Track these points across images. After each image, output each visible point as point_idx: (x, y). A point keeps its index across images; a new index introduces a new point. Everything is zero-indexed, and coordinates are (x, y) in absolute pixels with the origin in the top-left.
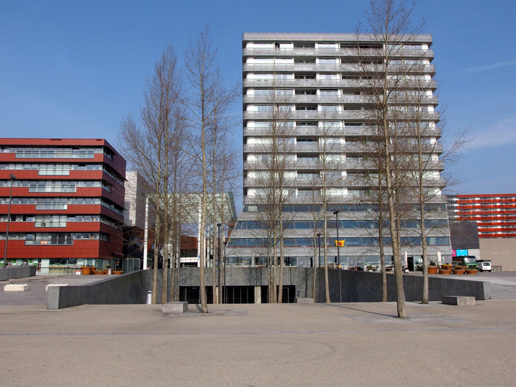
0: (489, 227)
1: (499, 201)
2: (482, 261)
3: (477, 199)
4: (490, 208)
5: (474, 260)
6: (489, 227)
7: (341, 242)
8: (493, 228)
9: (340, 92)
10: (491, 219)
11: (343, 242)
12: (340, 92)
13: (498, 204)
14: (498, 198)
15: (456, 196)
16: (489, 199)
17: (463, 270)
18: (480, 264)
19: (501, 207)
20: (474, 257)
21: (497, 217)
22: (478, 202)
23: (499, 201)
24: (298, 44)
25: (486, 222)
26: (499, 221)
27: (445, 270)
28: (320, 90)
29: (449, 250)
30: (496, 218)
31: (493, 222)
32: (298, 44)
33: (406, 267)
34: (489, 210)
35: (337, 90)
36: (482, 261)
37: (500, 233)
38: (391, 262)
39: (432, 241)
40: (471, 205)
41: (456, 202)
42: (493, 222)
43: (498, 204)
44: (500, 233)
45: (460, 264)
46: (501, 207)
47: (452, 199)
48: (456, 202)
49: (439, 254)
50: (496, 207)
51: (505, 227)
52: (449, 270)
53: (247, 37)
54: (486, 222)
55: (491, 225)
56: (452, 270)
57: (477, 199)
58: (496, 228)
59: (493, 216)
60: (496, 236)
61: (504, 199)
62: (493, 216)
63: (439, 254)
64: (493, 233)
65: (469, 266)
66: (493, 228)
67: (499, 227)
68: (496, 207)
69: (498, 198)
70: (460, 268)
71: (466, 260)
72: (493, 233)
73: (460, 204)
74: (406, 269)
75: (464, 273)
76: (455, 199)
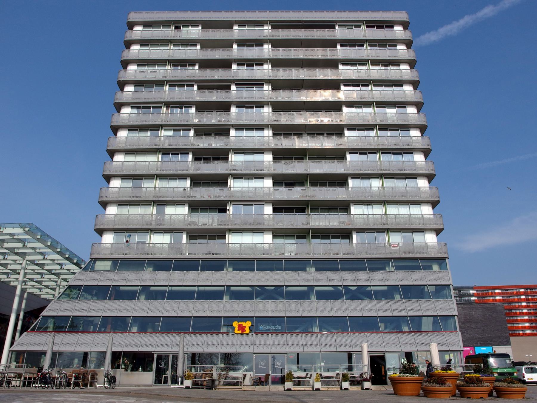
0: (515, 325)
1: (524, 294)
2: (522, 364)
3: (497, 291)
4: (514, 301)
5: (508, 361)
6: (515, 325)
7: (244, 324)
8: (520, 325)
9: (267, 88)
10: (516, 315)
11: (248, 324)
12: (267, 88)
13: (523, 297)
14: (522, 290)
15: (472, 288)
16: (511, 291)
17: (487, 386)
18: (519, 371)
19: (527, 300)
20: (506, 356)
21: (523, 313)
22: (499, 294)
23: (524, 294)
24: (207, 25)
25: (511, 318)
26: (526, 318)
27: (437, 387)
28: (236, 84)
29: (455, 341)
30: (523, 314)
31: (519, 318)
32: (207, 25)
33: (367, 376)
34: (513, 305)
35: (263, 84)
36: (522, 364)
37: (528, 332)
38: (347, 365)
39: (427, 324)
40: (491, 298)
41: (473, 295)
42: (519, 318)
43: (523, 297)
44: (528, 332)
45: (477, 370)
46: (527, 300)
47: (468, 292)
48: (473, 295)
49: (435, 349)
50: (520, 301)
51: (534, 325)
52: (450, 385)
53: (133, 17)
54: (511, 318)
55: (517, 321)
56: (458, 387)
57: (497, 291)
58: (523, 325)
59: (518, 311)
60: (525, 335)
61: (529, 291)
62: (518, 311)
63: (435, 349)
64: (521, 332)
65: (499, 374)
66: (520, 325)
67: (527, 325)
68: (520, 301)
69: (522, 290)
70: (479, 381)
71: (492, 361)
72: (521, 332)
73: (478, 297)
74: (366, 380)
75: (490, 395)
76: (472, 292)
